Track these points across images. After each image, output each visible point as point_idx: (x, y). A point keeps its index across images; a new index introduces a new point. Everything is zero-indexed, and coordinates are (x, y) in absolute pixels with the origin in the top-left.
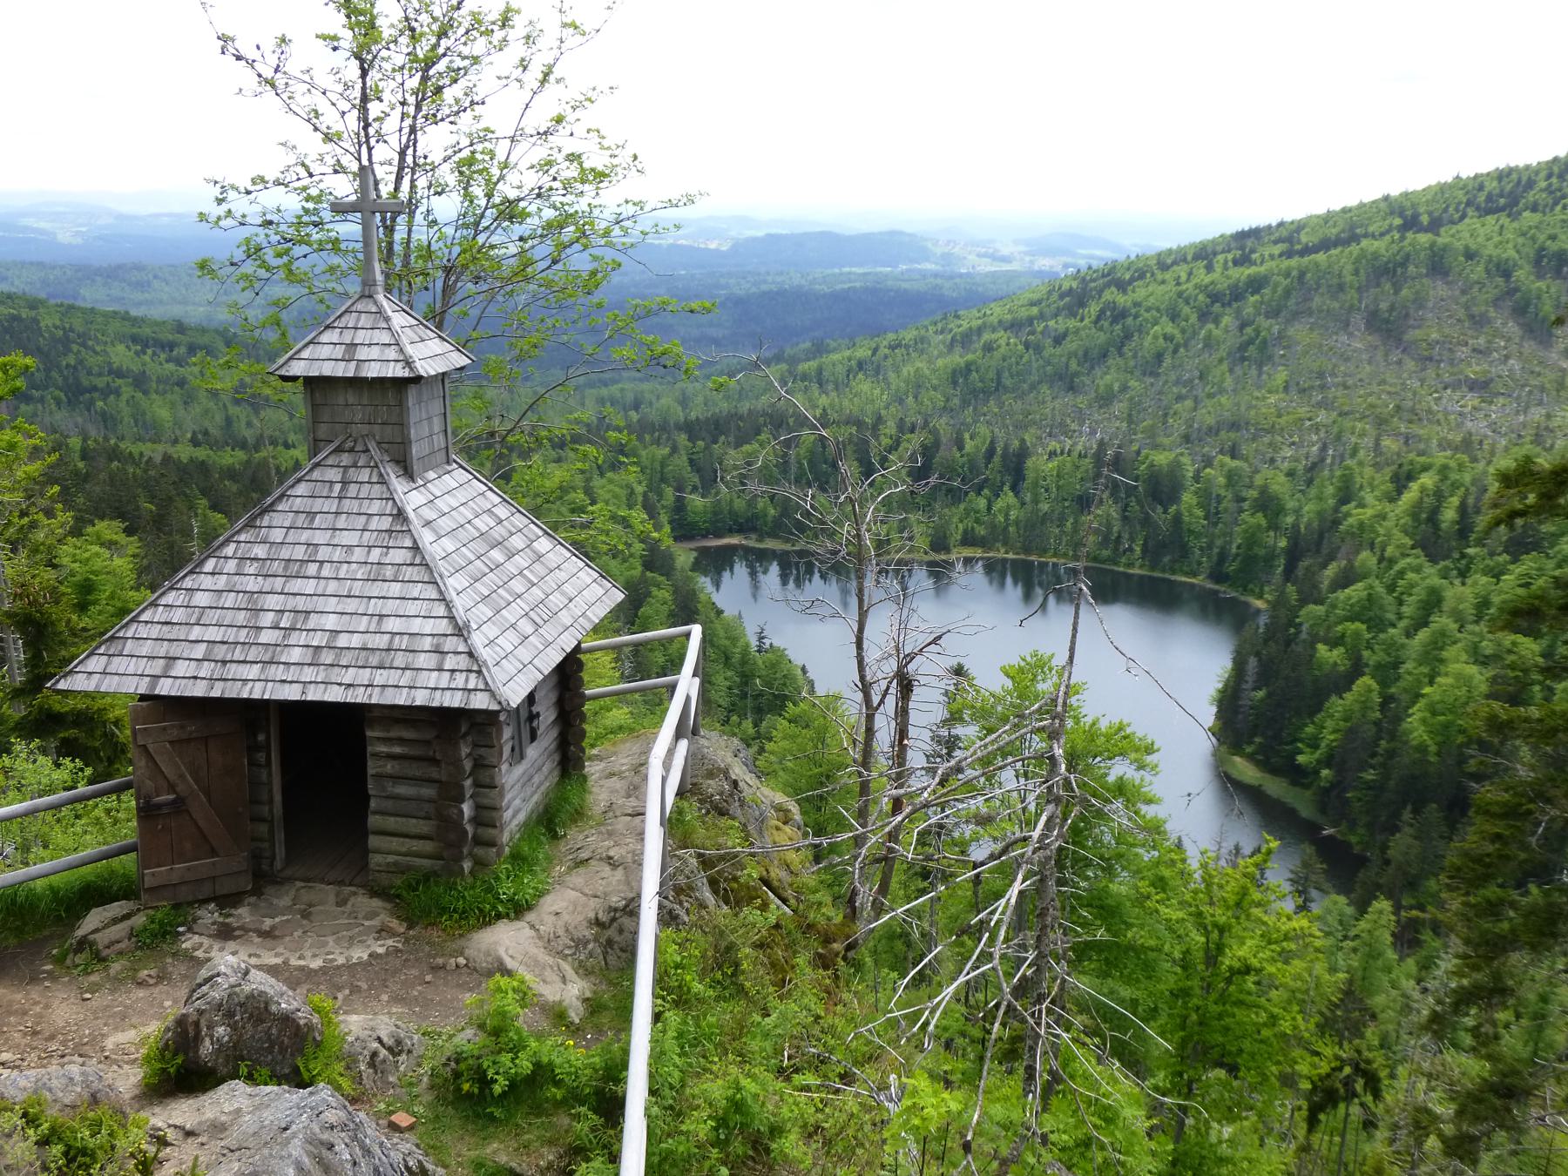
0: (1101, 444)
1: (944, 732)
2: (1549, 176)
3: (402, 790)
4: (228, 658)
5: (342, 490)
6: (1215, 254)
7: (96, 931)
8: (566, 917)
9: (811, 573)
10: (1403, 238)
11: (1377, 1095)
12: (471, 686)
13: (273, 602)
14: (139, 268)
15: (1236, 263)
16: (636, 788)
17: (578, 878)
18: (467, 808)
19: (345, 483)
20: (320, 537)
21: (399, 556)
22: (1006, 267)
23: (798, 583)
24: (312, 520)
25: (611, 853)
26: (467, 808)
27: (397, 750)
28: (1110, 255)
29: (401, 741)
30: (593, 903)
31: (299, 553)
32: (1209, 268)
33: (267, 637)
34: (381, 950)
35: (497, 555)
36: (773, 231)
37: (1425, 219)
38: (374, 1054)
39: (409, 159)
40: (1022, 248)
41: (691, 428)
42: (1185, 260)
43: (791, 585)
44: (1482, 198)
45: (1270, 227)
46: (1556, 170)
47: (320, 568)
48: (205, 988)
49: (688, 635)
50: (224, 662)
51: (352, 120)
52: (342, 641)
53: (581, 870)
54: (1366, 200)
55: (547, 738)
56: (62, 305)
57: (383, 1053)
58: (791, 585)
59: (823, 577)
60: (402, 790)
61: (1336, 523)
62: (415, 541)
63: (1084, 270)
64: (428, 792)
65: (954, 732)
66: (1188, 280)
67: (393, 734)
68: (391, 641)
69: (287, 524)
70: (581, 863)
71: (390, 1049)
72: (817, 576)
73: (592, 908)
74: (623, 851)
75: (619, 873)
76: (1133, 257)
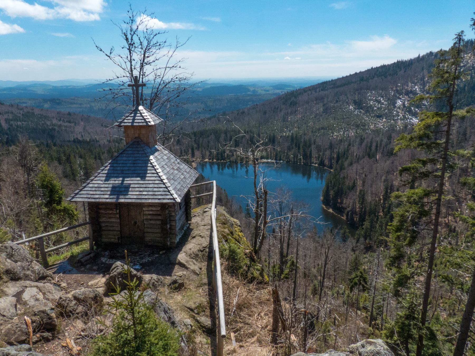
0: (292, 134)
2: (393, 67)
3: (151, 222)
6: (317, 88)
7: (82, 258)
8: (193, 250)
9: (225, 167)
10: (360, 83)
11: (366, 283)
14: (58, 99)
15: (322, 90)
16: (203, 219)
17: (194, 241)
18: (168, 226)
22: (268, 93)
23: (222, 169)
25: (201, 234)
26: (168, 226)
27: (151, 213)
28: (292, 89)
30: (199, 246)
32: (316, 92)
34: (150, 260)
36: (212, 86)
37: (365, 78)
38: (154, 283)
39: (142, 73)
40: (272, 88)
41: (195, 134)
42: (310, 90)
43: (220, 170)
44: (378, 73)
45: (329, 81)
48: (115, 269)
49: (213, 183)
51: (129, 64)
53: (194, 239)
54: (352, 74)
55: (183, 209)
57: (156, 283)
58: (220, 170)
59: (228, 168)
61: (348, 150)
63: (286, 93)
64: (159, 222)
70: (194, 237)
71: (157, 282)
72: (226, 168)
73: (198, 248)
74: (204, 234)
75: (204, 239)
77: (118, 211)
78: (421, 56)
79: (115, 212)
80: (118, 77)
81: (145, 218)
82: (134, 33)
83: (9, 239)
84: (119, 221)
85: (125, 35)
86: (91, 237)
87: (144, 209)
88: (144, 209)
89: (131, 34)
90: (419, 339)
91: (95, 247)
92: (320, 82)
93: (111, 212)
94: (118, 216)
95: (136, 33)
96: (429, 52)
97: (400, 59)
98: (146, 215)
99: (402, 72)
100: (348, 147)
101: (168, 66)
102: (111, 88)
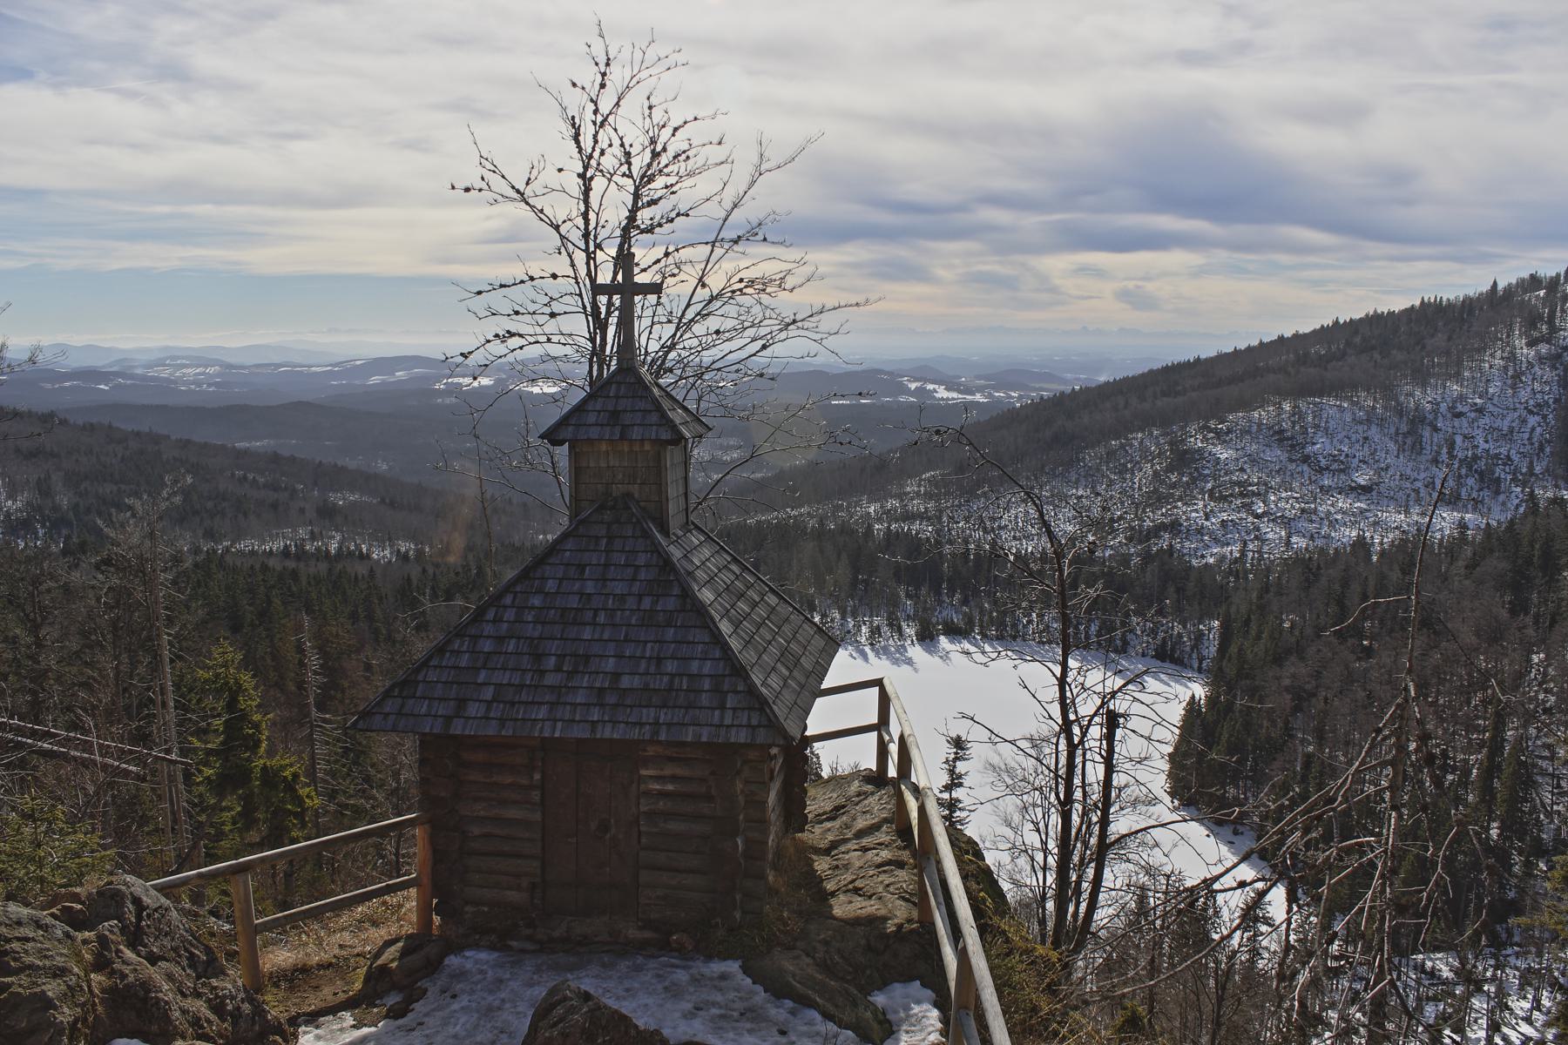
1: (946, 796)
3: (673, 826)
4: (517, 699)
5: (607, 544)
12: (754, 722)
13: (554, 647)
15: (1164, 394)
19: (610, 538)
20: (590, 587)
21: (671, 603)
24: (583, 571)
25: (858, 884)
28: (1059, 387)
29: (674, 779)
31: (573, 602)
33: (550, 679)
35: (743, 606)
44: (1358, 340)
46: (1413, 317)
47: (595, 615)
50: (513, 704)
52: (625, 682)
56: (181, 440)
60: (673, 826)
62: (683, 589)
65: (954, 795)
66: (1126, 407)
67: (668, 772)
68: (671, 682)
69: (560, 575)
76: (1006, 410)
77: (537, 776)
78: (1501, 285)
79: (525, 782)
80: (532, 279)
81: (643, 808)
82: (605, 120)
83: (1494, 636)
84: (538, 816)
85: (573, 125)
86: (426, 881)
87: (644, 772)
88: (644, 772)
89: (594, 123)
90: (356, 1008)
91: (437, 919)
92: (1157, 366)
93: (509, 780)
94: (536, 796)
95: (611, 119)
96: (1525, 275)
97: (1430, 296)
98: (648, 793)
99: (1440, 340)
100: (1260, 597)
101: (709, 247)
102: (517, 308)
